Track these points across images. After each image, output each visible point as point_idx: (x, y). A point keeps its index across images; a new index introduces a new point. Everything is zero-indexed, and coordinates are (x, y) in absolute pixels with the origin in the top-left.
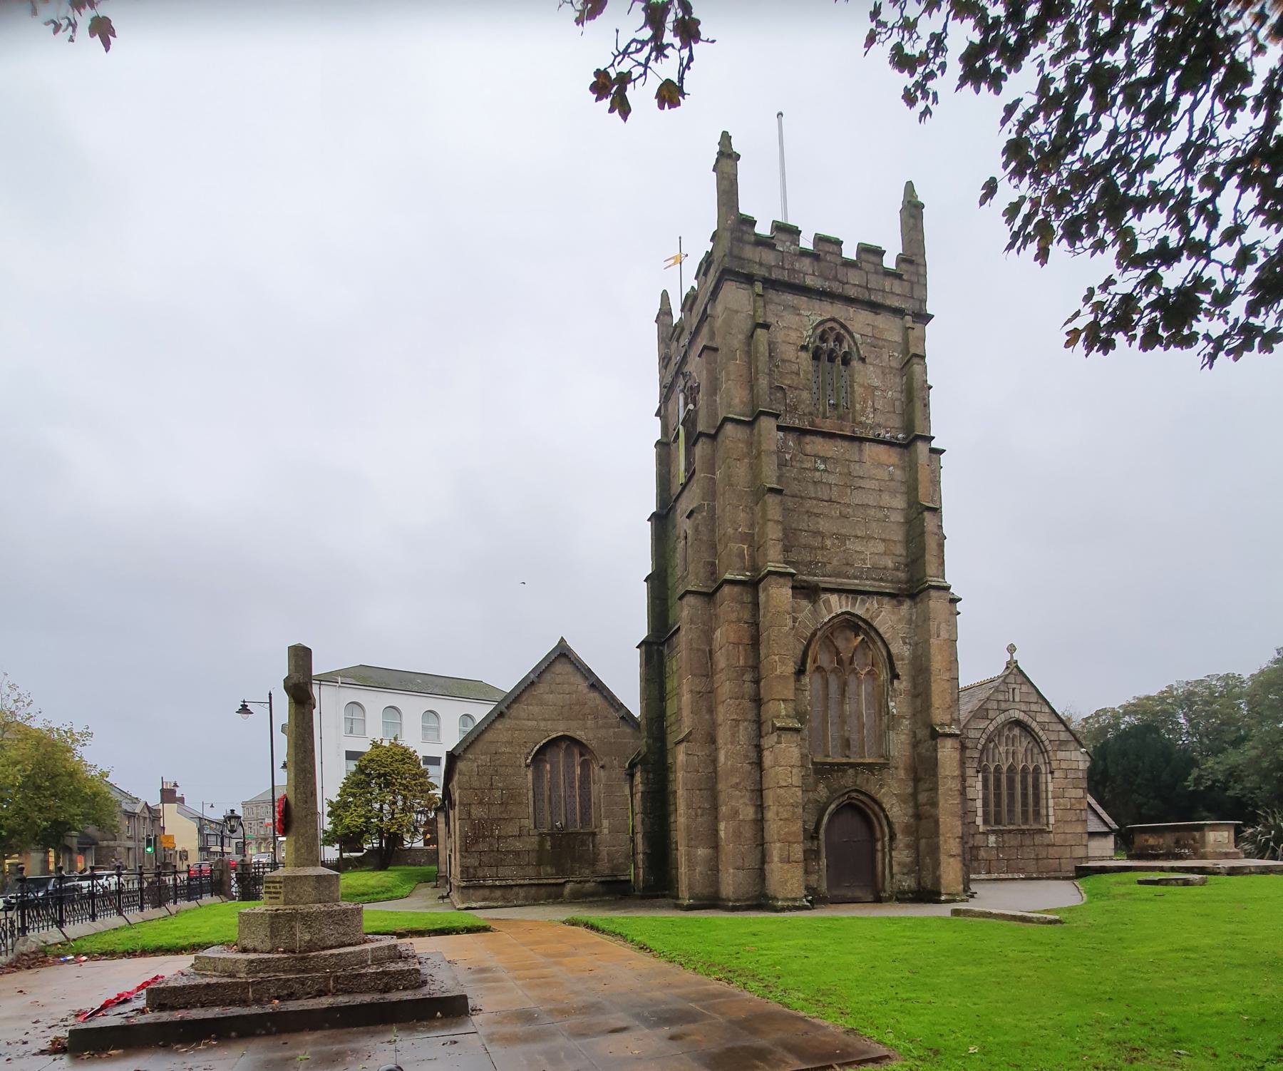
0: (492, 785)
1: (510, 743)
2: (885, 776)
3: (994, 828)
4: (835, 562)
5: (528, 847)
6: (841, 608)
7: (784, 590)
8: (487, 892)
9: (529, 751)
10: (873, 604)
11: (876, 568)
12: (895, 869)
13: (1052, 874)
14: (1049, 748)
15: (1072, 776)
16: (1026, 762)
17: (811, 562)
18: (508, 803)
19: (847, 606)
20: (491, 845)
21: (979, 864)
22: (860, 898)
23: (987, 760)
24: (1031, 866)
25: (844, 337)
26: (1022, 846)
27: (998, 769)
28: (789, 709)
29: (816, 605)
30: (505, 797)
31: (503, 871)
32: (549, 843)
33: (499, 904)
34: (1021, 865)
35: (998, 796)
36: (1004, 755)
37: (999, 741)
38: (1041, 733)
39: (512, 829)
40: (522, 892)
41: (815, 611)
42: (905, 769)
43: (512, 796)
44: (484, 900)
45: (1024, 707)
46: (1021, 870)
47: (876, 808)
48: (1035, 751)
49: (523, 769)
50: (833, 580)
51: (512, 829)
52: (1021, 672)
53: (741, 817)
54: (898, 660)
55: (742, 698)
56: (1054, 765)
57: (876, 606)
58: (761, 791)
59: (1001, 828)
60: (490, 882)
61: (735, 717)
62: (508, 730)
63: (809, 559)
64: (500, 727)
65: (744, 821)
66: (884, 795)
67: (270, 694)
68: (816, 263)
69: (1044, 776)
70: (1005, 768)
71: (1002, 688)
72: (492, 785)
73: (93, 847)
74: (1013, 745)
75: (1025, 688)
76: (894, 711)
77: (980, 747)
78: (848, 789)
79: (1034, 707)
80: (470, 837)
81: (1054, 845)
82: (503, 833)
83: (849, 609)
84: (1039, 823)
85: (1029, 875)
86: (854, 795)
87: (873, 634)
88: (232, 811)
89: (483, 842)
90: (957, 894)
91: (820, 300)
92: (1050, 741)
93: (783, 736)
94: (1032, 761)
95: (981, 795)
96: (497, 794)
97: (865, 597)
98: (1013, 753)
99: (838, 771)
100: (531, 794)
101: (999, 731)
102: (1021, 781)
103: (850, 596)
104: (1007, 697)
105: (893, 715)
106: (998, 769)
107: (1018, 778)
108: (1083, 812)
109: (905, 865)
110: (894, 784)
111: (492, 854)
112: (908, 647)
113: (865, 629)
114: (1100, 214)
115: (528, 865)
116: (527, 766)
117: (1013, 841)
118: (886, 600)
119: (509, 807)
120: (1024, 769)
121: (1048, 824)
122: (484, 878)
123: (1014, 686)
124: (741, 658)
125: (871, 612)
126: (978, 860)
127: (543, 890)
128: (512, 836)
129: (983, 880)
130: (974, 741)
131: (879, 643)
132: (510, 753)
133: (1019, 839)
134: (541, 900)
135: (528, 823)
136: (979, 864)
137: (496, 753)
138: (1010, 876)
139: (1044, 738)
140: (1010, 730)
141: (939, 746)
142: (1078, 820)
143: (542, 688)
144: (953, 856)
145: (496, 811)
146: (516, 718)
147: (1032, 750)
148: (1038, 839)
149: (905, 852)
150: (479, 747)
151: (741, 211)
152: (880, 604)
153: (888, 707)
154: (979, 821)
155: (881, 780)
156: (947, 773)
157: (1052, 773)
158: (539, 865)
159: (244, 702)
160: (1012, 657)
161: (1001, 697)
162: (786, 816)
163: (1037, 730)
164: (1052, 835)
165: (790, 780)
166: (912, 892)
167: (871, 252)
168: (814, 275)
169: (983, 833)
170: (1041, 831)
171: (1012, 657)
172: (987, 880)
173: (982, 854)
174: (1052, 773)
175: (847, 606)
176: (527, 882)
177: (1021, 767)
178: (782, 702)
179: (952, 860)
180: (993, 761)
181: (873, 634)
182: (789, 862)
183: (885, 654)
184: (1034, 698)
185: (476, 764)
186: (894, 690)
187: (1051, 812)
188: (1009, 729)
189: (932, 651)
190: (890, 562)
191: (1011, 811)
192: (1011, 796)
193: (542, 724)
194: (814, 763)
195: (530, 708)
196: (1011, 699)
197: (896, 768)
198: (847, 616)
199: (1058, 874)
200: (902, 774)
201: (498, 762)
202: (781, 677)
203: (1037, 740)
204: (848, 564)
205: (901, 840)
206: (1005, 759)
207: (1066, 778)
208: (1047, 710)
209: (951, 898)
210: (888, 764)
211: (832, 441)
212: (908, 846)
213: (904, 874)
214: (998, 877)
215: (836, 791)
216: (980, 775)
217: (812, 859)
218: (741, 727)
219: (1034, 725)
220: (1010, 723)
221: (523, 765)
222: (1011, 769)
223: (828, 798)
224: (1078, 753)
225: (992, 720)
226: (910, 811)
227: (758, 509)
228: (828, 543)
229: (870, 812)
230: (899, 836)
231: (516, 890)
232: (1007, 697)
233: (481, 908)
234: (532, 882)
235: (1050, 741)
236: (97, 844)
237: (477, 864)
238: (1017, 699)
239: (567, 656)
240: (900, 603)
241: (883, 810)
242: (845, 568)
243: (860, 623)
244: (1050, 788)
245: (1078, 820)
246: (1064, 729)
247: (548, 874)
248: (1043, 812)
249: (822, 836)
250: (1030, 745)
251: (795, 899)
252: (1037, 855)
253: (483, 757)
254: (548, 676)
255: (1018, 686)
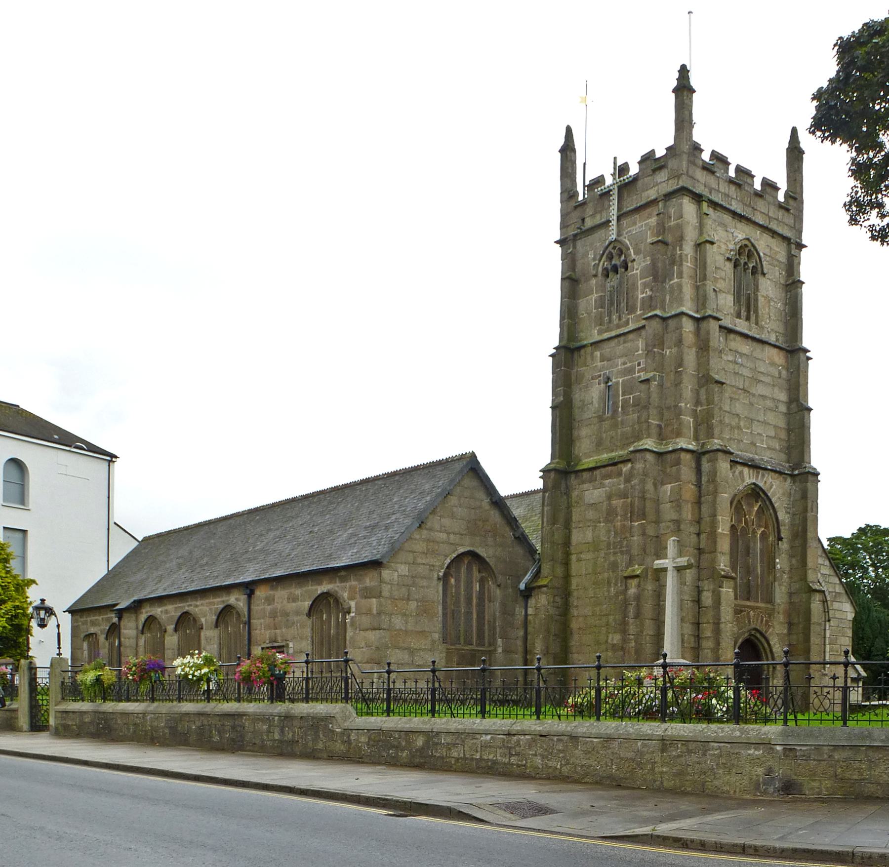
6: (749, 478)
19: (753, 478)
25: (753, 254)
49: (435, 582)
58: (698, 624)
66: (770, 634)
68: (738, 190)
88: (43, 601)
91: (740, 221)
110: (777, 627)
113: (763, 498)
114: (871, 105)
116: (439, 579)
151: (694, 139)
167: (769, 185)
168: (736, 199)
175: (753, 478)
211: (746, 340)
227: (703, 391)
228: (742, 424)
229: (761, 647)
239: (476, 470)
243: (761, 493)
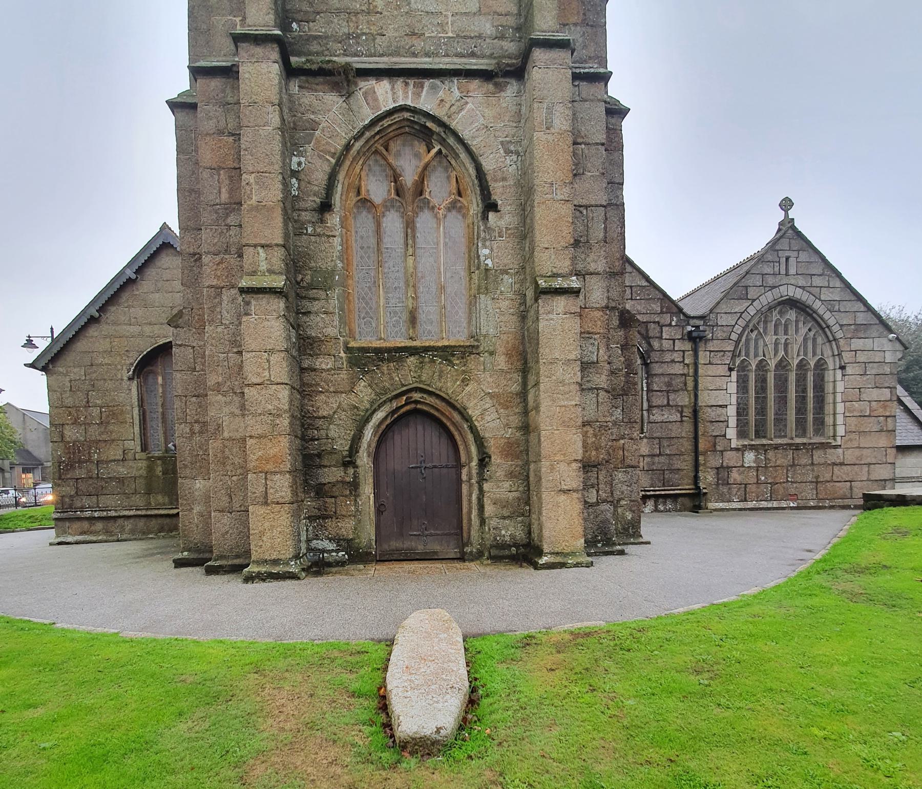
0: (88, 402)
1: (109, 352)
2: (471, 365)
3: (753, 443)
4: (390, 33)
5: (134, 473)
7: (264, 65)
8: (86, 525)
9: (132, 361)
10: (452, 90)
11: (465, 37)
12: (489, 509)
13: (840, 502)
14: (839, 335)
15: (874, 372)
16: (806, 354)
17: (348, 36)
18: (108, 423)
20: (89, 471)
21: (730, 489)
22: (435, 553)
23: (747, 355)
24: (808, 492)
26: (793, 465)
27: (762, 366)
28: (274, 260)
29: (352, 100)
30: (104, 415)
31: (104, 501)
32: (160, 469)
33: (100, 538)
34: (792, 491)
35: (761, 400)
36: (771, 347)
37: (765, 329)
38: (827, 316)
39: (114, 452)
40: (129, 525)
41: (350, 109)
42: (508, 355)
43: (112, 414)
44: (83, 533)
45: (801, 282)
46: (793, 497)
47: (457, 417)
48: (820, 340)
49: (126, 383)
50: (385, 59)
51: (114, 452)
52: (799, 235)
53: (226, 435)
54: (496, 181)
55: (227, 251)
56: (847, 357)
57: (457, 93)
59: (764, 441)
60: (88, 514)
61: (215, 282)
62: (105, 337)
63: (346, 31)
64: (96, 334)
65: (231, 439)
67: (52, 329)
69: (831, 372)
70: (772, 364)
71: (769, 257)
72: (88, 402)
73: (40, 467)
74: (786, 333)
75: (804, 256)
76: (489, 262)
77: (734, 337)
78: (404, 388)
79: (817, 281)
80: (64, 462)
81: (842, 464)
82: (104, 457)
83: (409, 103)
84: (823, 435)
85: (802, 503)
86: (416, 396)
87: (451, 141)
89: (80, 468)
90: (573, 554)
92: (841, 326)
93: (253, 302)
94: (814, 354)
95: (734, 400)
96: (95, 412)
97: (437, 82)
98: (786, 345)
99: (389, 360)
100: (136, 411)
101: (765, 314)
102: (797, 381)
103: (411, 82)
104: (777, 269)
105: (487, 270)
106: (762, 366)
107: (792, 377)
108: (889, 419)
109: (504, 504)
111: (90, 482)
112: (514, 157)
115: (135, 492)
117: (781, 459)
118: (475, 84)
119: (111, 427)
120: (802, 365)
121: (834, 436)
122: (82, 509)
123: (787, 254)
124: (223, 190)
125: (448, 105)
126: (728, 484)
127: (153, 523)
128: (115, 461)
129: (735, 509)
130: (725, 329)
131: (463, 155)
132: (110, 365)
133: (790, 456)
134: (151, 533)
135: (135, 445)
136: (730, 489)
137: (92, 365)
138: (775, 504)
139: (831, 322)
140: (781, 313)
141: (541, 311)
142: (881, 431)
143: (145, 286)
144: (565, 492)
145: (94, 432)
146: (115, 323)
147: (814, 340)
148: (818, 456)
149: (507, 485)
150: (71, 357)
152: (465, 94)
153: (478, 257)
154: (731, 433)
155: (464, 372)
156: (557, 355)
157: (842, 368)
158: (149, 492)
159: (29, 337)
160: (787, 215)
161: (767, 269)
162: (260, 432)
163: (821, 312)
164: (840, 451)
165: (266, 374)
166: (516, 545)
169: (737, 449)
170: (824, 446)
171: (787, 215)
172: (740, 510)
173: (735, 476)
174: (842, 368)
176: (132, 513)
177: (796, 362)
178: (261, 250)
179: (563, 497)
180: (756, 355)
181: (451, 141)
182: (266, 503)
183: (472, 171)
184: (817, 269)
185: (68, 379)
186: (488, 229)
187: (840, 419)
188: (781, 313)
189: (537, 154)
190: (488, 25)
191: (780, 420)
192: (782, 400)
193: (147, 329)
194: (348, 349)
195: (132, 310)
196: (783, 272)
197: (492, 353)
198: (407, 115)
199: (847, 502)
200: (501, 362)
201: (95, 375)
202: (259, 208)
203: (822, 327)
204: (414, 34)
205: (499, 464)
206: (772, 353)
207: (865, 374)
208: (838, 284)
209: (559, 559)
210: (478, 347)
212: (511, 475)
213: (504, 518)
214: (757, 506)
215: (385, 391)
216: (734, 374)
217: (346, 496)
218: (225, 298)
219: (817, 305)
220: (780, 303)
221: (125, 378)
222: (782, 365)
223: (372, 403)
224: (884, 341)
225: (754, 300)
226: (515, 420)
230: (496, 459)
231: (120, 521)
232: (777, 269)
233: (77, 543)
234: (139, 513)
235: (841, 326)
236: (42, 464)
237: (73, 493)
238: (792, 271)
240: (500, 87)
241: (467, 419)
242: (409, 41)
243: (429, 124)
244: (840, 387)
245: (881, 431)
246: (863, 308)
247: (159, 504)
248: (829, 420)
249: (364, 460)
250: (812, 334)
251: (276, 562)
252: (817, 477)
253: (76, 370)
254: (151, 272)
255: (795, 254)
